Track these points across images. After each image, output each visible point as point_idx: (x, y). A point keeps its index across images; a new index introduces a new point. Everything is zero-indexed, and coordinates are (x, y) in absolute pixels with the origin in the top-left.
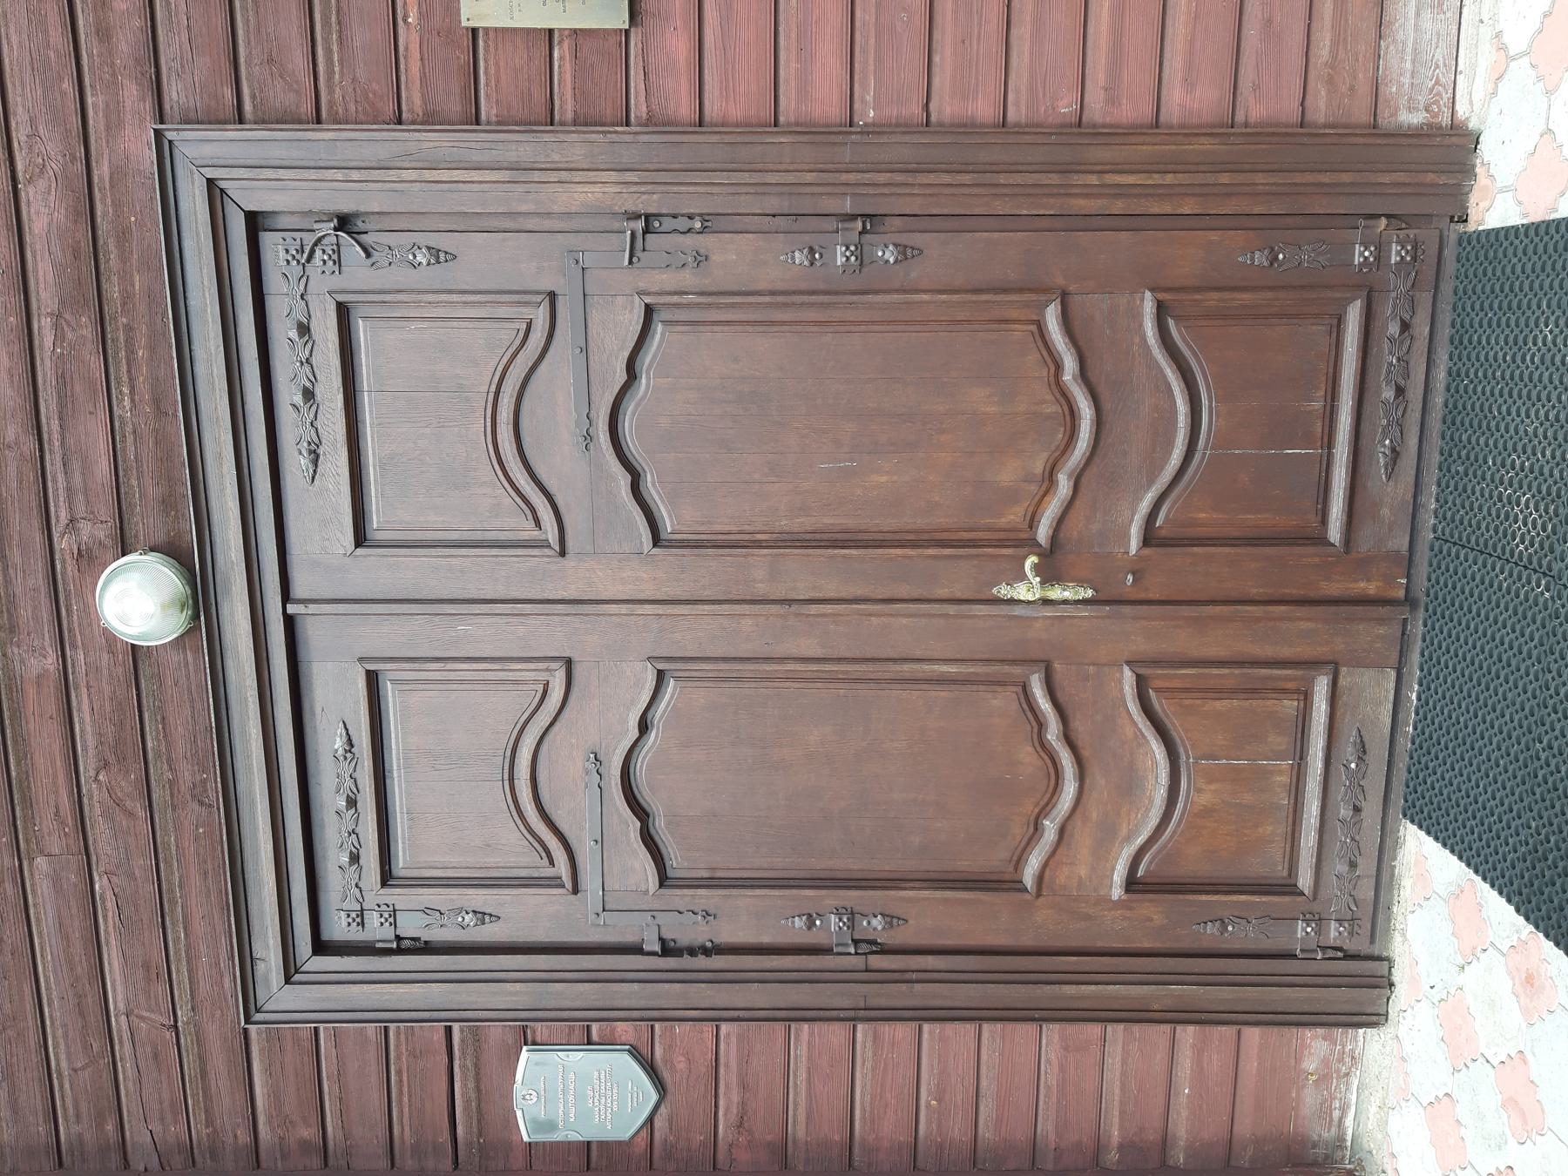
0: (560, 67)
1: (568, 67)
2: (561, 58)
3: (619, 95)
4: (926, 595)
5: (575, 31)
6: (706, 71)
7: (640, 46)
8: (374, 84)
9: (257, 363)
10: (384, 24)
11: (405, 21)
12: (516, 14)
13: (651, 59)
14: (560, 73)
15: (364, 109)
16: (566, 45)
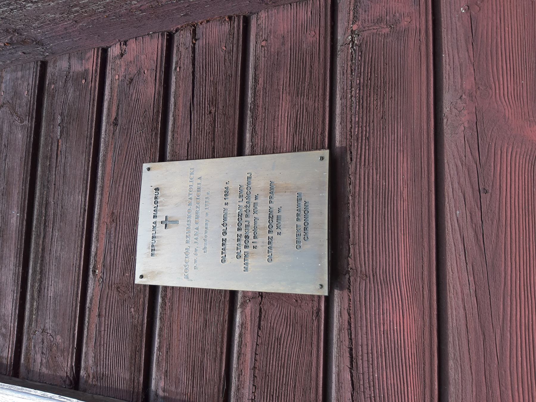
0: (240, 335)
1: (248, 338)
2: (243, 325)
3: (313, 384)
4: (477, 149)
5: (261, 295)
6: (451, 363)
7: (346, 317)
8: (58, 337)
9: (327, 241)
10: (76, 275)
11: (94, 272)
12: (191, 273)
13: (361, 339)
14: (240, 343)
15: (48, 361)
16: (248, 310)
